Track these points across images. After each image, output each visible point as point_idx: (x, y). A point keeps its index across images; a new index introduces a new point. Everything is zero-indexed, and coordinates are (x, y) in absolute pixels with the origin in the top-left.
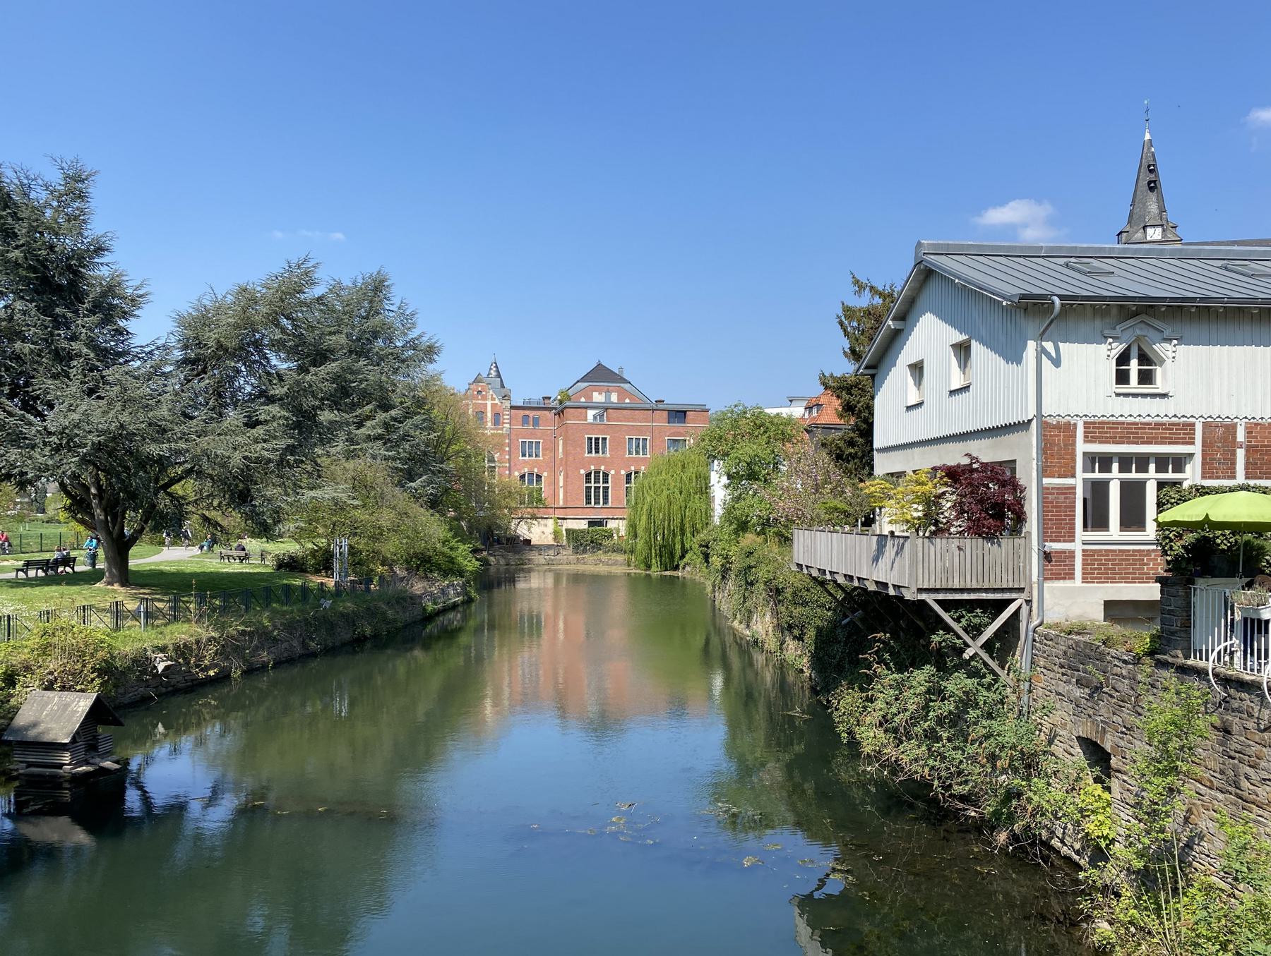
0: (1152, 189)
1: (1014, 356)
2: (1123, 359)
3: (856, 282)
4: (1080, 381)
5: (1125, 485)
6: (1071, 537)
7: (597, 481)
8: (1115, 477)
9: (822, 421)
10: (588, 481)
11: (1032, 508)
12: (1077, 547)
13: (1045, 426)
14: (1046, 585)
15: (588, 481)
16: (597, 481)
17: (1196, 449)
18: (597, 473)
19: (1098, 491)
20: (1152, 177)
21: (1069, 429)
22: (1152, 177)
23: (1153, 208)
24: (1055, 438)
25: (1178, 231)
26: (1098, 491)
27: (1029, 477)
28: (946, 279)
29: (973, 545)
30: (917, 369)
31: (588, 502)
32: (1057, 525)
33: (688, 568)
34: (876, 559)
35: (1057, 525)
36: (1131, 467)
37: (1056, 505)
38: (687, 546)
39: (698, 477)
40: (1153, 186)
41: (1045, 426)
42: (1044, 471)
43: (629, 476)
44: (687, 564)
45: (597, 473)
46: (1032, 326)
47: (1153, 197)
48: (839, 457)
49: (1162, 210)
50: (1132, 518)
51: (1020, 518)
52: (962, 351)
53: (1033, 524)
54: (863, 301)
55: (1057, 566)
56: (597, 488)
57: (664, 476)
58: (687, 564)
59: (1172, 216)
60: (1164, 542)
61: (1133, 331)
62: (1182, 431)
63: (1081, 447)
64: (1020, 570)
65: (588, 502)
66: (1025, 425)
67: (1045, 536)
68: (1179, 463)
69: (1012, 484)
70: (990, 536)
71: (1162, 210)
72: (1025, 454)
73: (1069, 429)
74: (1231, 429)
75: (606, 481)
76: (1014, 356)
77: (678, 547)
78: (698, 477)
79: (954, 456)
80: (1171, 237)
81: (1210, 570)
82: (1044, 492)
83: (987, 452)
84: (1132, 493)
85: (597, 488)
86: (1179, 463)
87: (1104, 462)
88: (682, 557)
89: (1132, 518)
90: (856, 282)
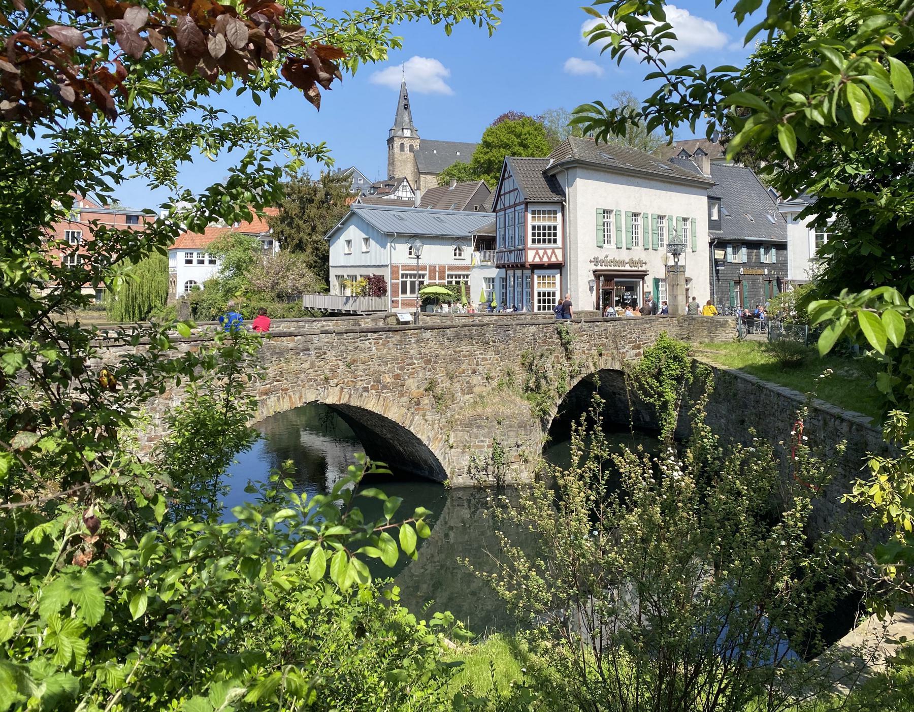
1: (384, 246)
2: (410, 248)
4: (400, 254)
5: (411, 282)
8: (409, 280)
11: (389, 289)
12: (400, 299)
13: (392, 266)
14: (560, 259)
17: (427, 272)
19: (404, 284)
20: (405, 102)
21: (398, 267)
22: (405, 102)
23: (406, 119)
24: (395, 270)
26: (404, 284)
27: (388, 279)
29: (376, 299)
30: (349, 242)
37: (394, 286)
40: (406, 107)
41: (392, 266)
42: (392, 279)
44: (153, 316)
47: (406, 113)
49: (411, 121)
50: (412, 291)
51: (385, 291)
52: (366, 240)
53: (389, 293)
58: (153, 316)
59: (414, 124)
61: (411, 240)
63: (401, 272)
64: (386, 305)
66: (387, 266)
67: (392, 296)
68: (423, 276)
69: (384, 282)
71: (411, 121)
73: (398, 267)
76: (384, 246)
79: (371, 272)
81: (429, 303)
82: (392, 284)
83: (378, 272)
86: (423, 276)
87: (406, 276)
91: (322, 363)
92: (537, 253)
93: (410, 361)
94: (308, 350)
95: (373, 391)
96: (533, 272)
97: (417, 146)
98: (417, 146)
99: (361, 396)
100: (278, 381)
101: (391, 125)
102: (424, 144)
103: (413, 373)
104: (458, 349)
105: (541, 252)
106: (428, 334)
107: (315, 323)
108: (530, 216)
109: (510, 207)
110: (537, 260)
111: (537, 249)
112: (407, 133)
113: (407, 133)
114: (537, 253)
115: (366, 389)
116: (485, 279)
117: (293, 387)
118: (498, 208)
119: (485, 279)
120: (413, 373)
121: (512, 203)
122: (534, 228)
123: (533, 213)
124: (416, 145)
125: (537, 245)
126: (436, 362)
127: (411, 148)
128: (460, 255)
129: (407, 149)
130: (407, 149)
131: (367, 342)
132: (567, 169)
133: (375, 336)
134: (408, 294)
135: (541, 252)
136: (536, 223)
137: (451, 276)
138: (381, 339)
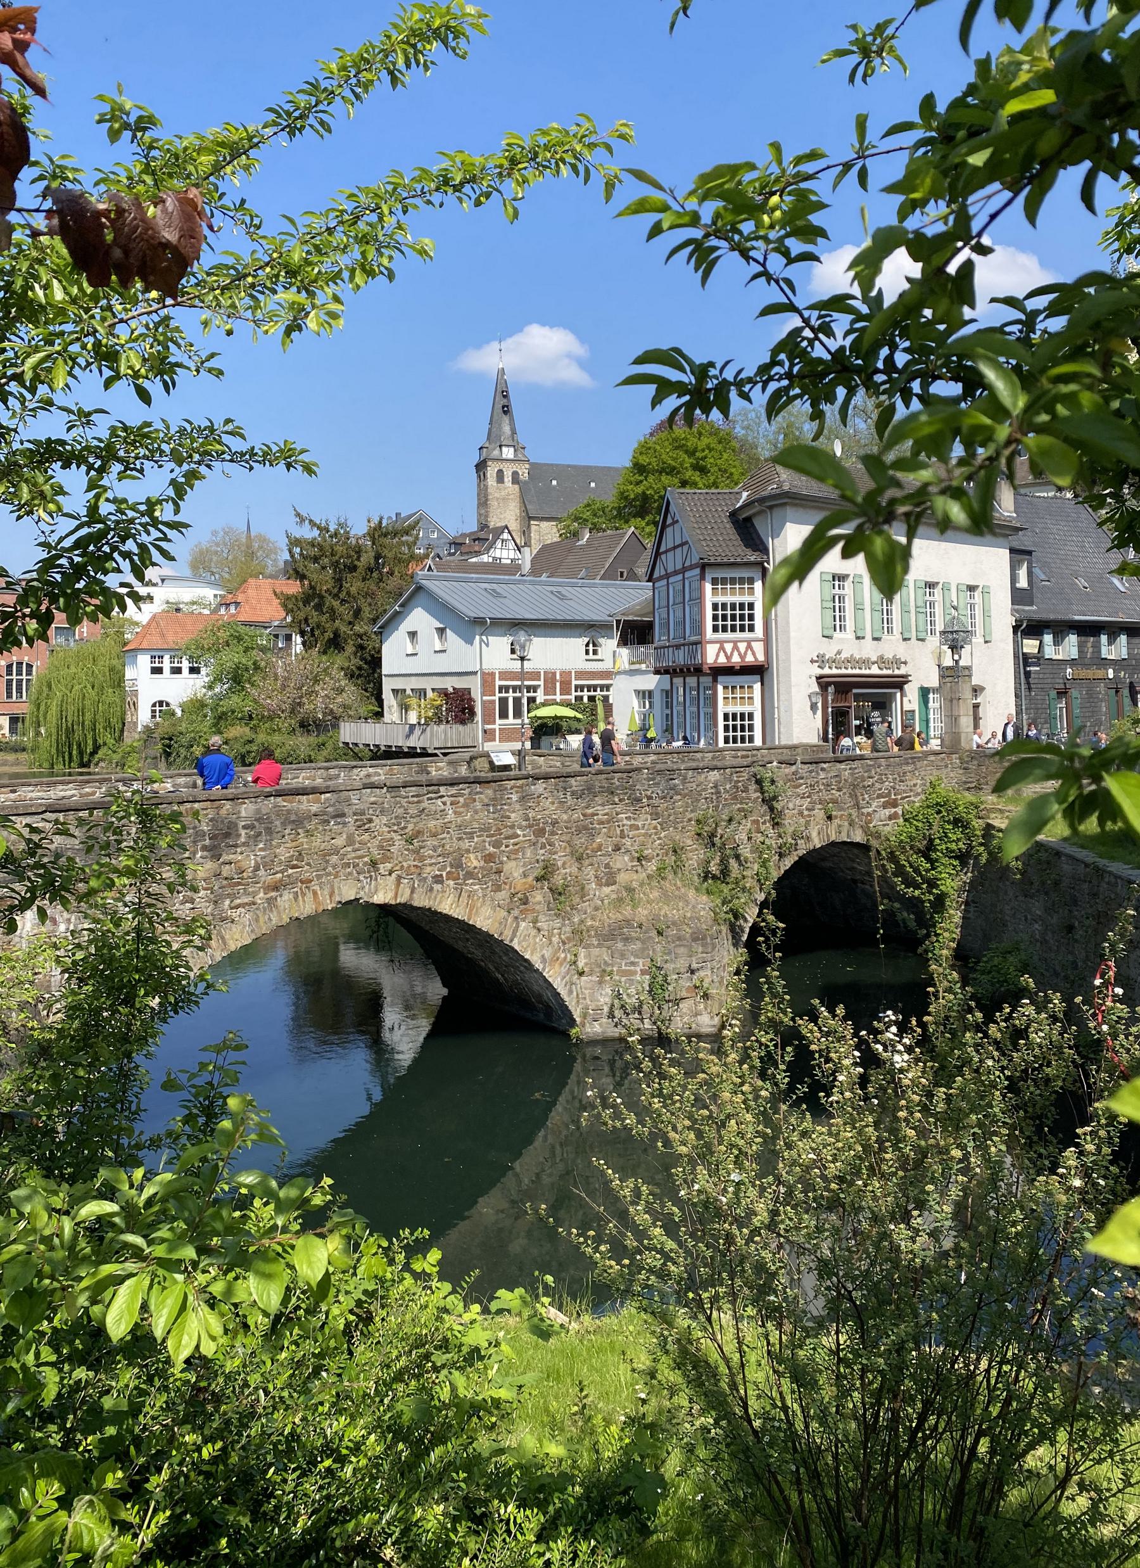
0: (505, 413)
1: (470, 641)
3: (298, 515)
4: (496, 653)
6: (494, 722)
7: (19, 673)
9: (242, 618)
10: (9, 673)
11: (478, 709)
12: (497, 727)
13: (483, 674)
14: (761, 658)
15: (9, 673)
16: (19, 673)
17: (541, 683)
18: (20, 664)
19: (503, 702)
21: (493, 674)
23: (507, 429)
24: (488, 679)
25: (526, 452)
26: (503, 702)
27: (476, 694)
28: (430, 595)
30: (413, 635)
31: (9, 695)
32: (488, 718)
33: (102, 764)
34: (408, 736)
35: (488, 718)
36: (517, 693)
37: (488, 707)
38: (101, 742)
39: (112, 669)
40: (506, 410)
41: (483, 674)
42: (483, 694)
43: (9, 667)
45: (20, 664)
46: (478, 629)
47: (506, 419)
48: (352, 676)
49: (514, 432)
50: (518, 714)
51: (472, 713)
52: (441, 631)
53: (479, 717)
54: (308, 533)
55: (488, 735)
56: (20, 682)
57: (73, 670)
59: (521, 438)
60: (531, 723)
62: (535, 675)
63: (498, 683)
64: (475, 738)
65: (9, 695)
66: (475, 673)
67: (485, 722)
68: (535, 689)
69: (471, 699)
70: (463, 722)
71: (514, 432)
72: (475, 686)
73: (493, 674)
74: (554, 674)
75: (29, 673)
76: (470, 641)
77: (90, 742)
78: (112, 669)
80: (520, 457)
81: (545, 734)
84: (517, 702)
85: (20, 682)
86: (535, 689)
88: (94, 752)
89: (518, 714)
90: (298, 515)
91: (366, 837)
92: (722, 648)
93: (510, 832)
94: (343, 815)
95: (451, 883)
96: (715, 681)
97: (524, 475)
98: (524, 475)
99: (431, 889)
100: (294, 867)
101: (482, 440)
102: (536, 470)
103: (516, 852)
104: (590, 811)
105: (728, 647)
106: (540, 787)
107: (355, 771)
108: (708, 587)
109: (676, 573)
110: (722, 660)
111: (721, 643)
112: (508, 453)
113: (508, 453)
114: (722, 648)
115: (438, 879)
116: (637, 692)
117: (319, 877)
118: (656, 575)
119: (637, 692)
120: (516, 852)
121: (679, 566)
122: (715, 607)
123: (714, 581)
124: (524, 472)
125: (721, 635)
126: (553, 833)
127: (515, 478)
128: (595, 652)
129: (508, 478)
130: (508, 478)
131: (439, 802)
132: (771, 508)
133: (453, 790)
134: (511, 720)
135: (728, 647)
136: (720, 599)
137: (580, 688)
138: (462, 795)
